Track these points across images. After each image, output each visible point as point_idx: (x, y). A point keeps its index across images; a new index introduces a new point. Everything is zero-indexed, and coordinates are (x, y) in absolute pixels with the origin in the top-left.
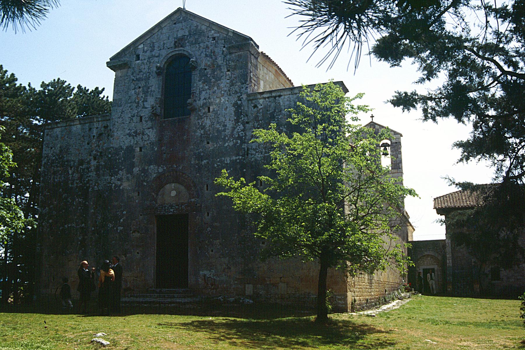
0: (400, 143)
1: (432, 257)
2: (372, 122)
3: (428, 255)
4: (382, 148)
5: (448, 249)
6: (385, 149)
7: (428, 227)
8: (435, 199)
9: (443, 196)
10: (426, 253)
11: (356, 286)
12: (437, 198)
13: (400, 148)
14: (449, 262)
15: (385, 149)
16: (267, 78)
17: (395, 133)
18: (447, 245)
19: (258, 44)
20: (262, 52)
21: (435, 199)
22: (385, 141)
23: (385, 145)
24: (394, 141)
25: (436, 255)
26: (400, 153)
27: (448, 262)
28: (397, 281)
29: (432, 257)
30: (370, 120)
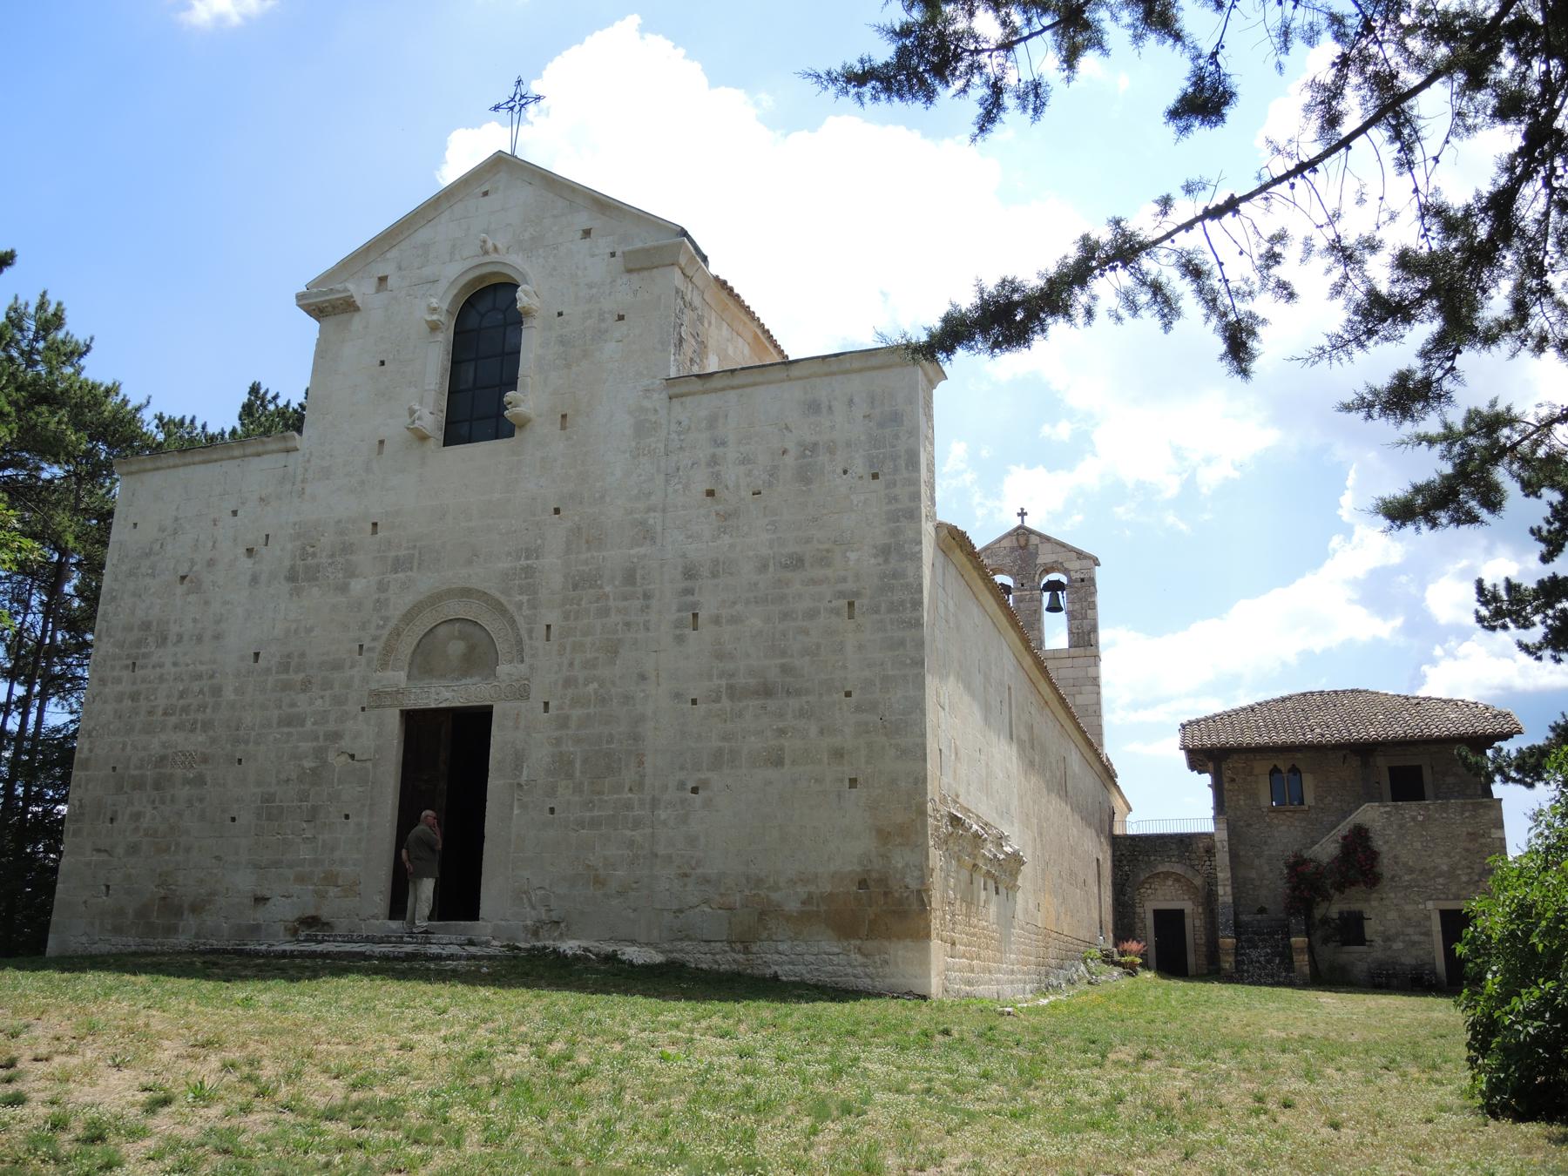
0: (1092, 581)
1: (1178, 878)
2: (1019, 527)
3: (1167, 875)
4: (1047, 595)
5: (1222, 858)
6: (1055, 598)
7: (1170, 799)
8: (1183, 726)
9: (1206, 719)
10: (1161, 869)
11: (959, 927)
12: (1190, 723)
13: (1094, 593)
14: (1224, 893)
15: (1055, 598)
16: (730, 351)
17: (1081, 555)
18: (1218, 845)
19: (705, 252)
20: (717, 278)
21: (1183, 726)
22: (1054, 577)
23: (1054, 587)
24: (1075, 576)
25: (1190, 874)
26: (1093, 606)
27: (1221, 892)
28: (1084, 934)
29: (1178, 878)
30: (1017, 522)
